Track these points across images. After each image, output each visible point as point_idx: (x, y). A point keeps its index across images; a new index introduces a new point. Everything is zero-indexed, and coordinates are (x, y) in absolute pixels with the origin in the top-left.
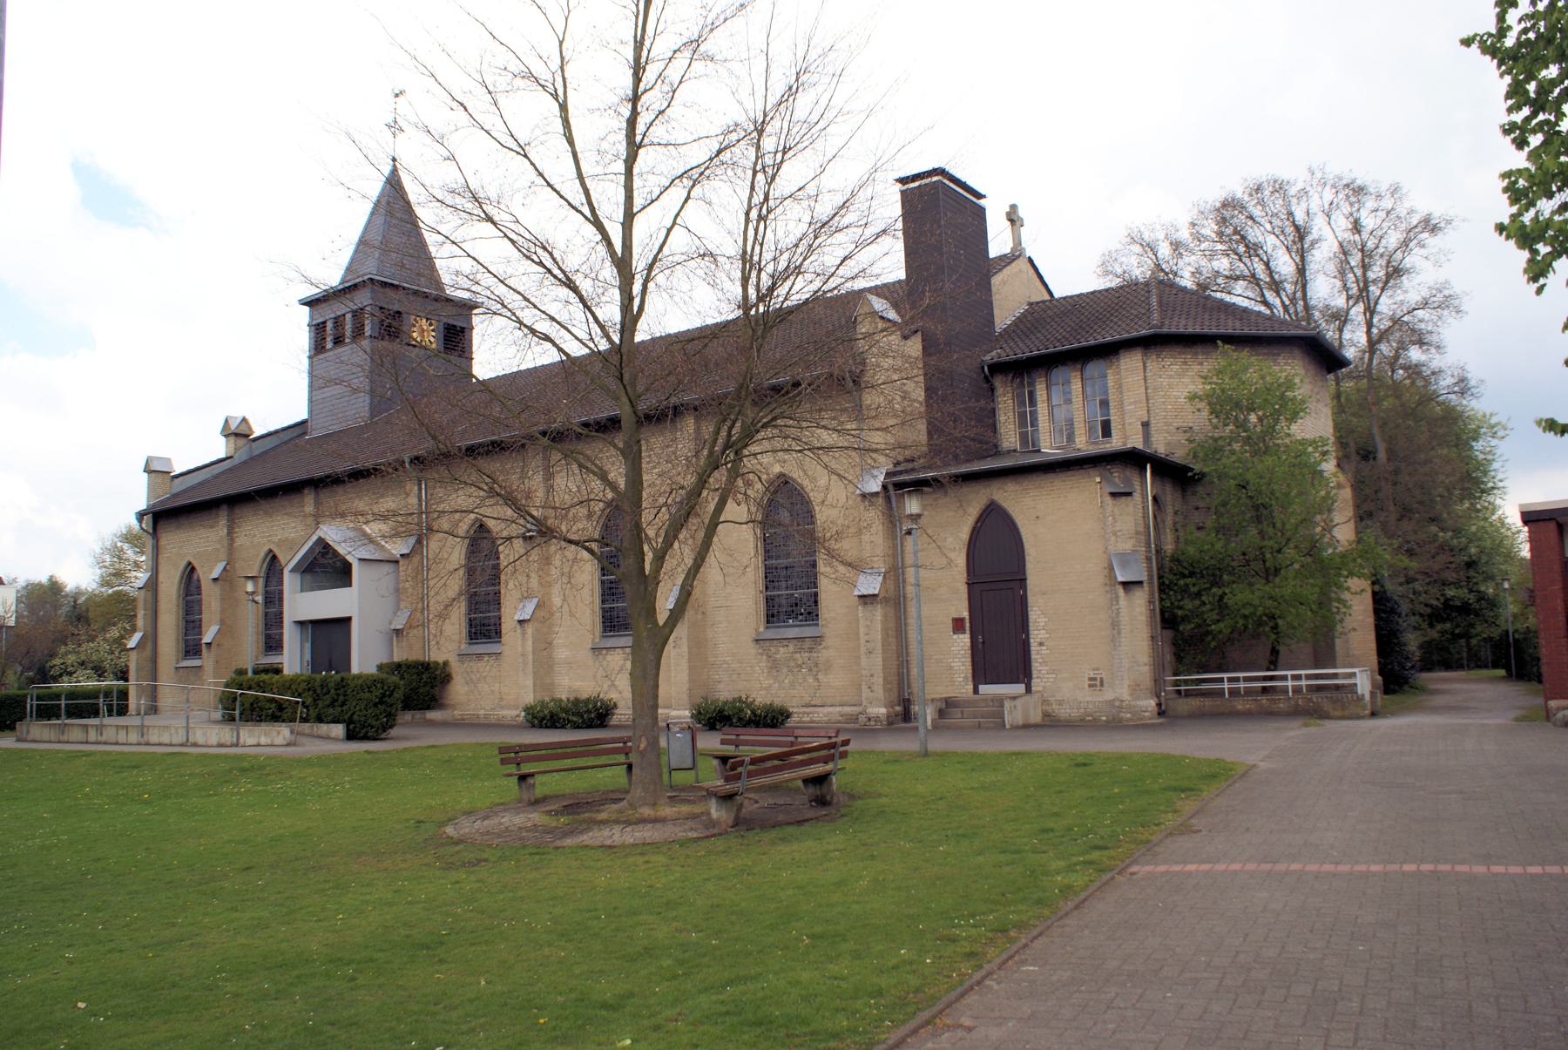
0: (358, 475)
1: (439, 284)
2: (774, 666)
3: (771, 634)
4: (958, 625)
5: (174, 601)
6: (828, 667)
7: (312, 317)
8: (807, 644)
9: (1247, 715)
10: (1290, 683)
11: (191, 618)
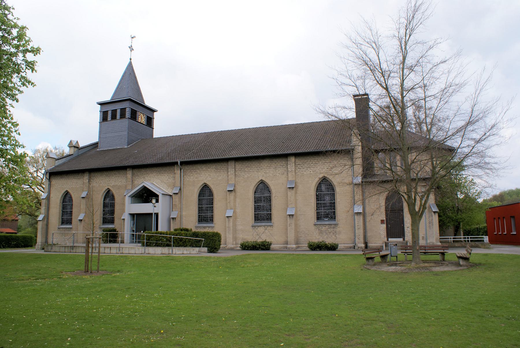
0: (334, 151)
1: (144, 103)
2: (321, 232)
3: (319, 223)
4: (382, 222)
5: (58, 204)
6: (340, 233)
7: (101, 108)
8: (333, 226)
9: (459, 247)
10: (470, 239)
11: (64, 210)
